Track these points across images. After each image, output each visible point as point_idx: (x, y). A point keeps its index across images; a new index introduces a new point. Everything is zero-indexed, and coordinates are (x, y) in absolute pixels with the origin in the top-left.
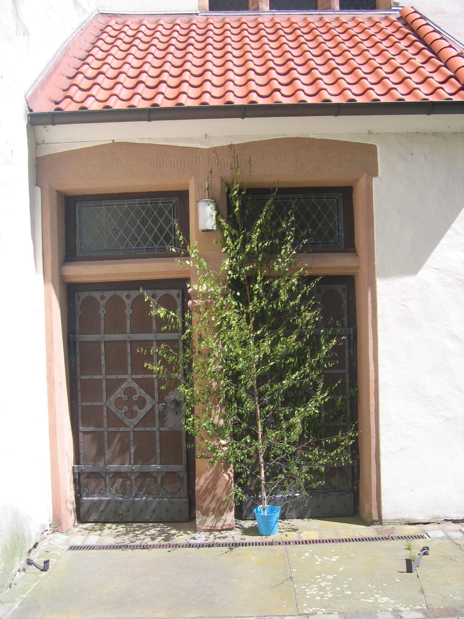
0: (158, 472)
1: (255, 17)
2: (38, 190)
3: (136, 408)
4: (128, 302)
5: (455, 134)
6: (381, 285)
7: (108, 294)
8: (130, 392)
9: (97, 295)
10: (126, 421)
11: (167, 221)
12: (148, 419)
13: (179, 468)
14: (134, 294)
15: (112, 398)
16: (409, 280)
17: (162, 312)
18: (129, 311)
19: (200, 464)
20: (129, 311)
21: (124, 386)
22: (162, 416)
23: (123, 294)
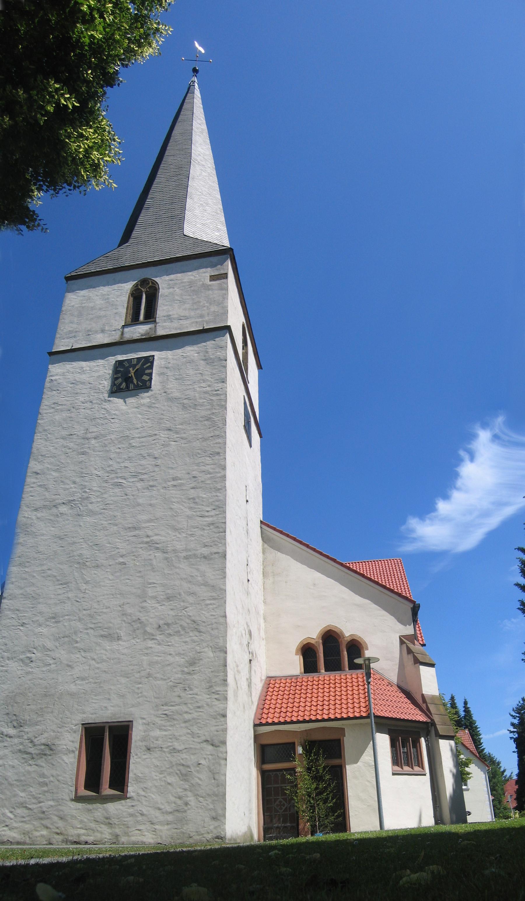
0: (289, 826)
1: (318, 676)
2: (255, 744)
3: (282, 807)
4: (279, 775)
5: (366, 724)
6: (347, 766)
7: (274, 773)
8: (280, 802)
9: (271, 773)
10: (279, 811)
11: (290, 751)
12: (285, 810)
13: (295, 825)
14: (281, 773)
15: (276, 804)
16: (355, 765)
17: (289, 777)
18: (280, 778)
19: (300, 821)
20: (280, 778)
21: (279, 800)
22: (290, 809)
23: (278, 773)
